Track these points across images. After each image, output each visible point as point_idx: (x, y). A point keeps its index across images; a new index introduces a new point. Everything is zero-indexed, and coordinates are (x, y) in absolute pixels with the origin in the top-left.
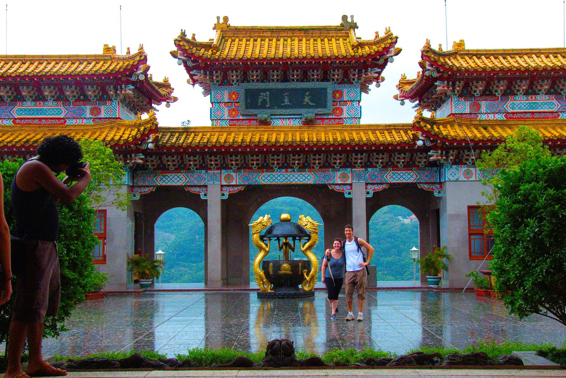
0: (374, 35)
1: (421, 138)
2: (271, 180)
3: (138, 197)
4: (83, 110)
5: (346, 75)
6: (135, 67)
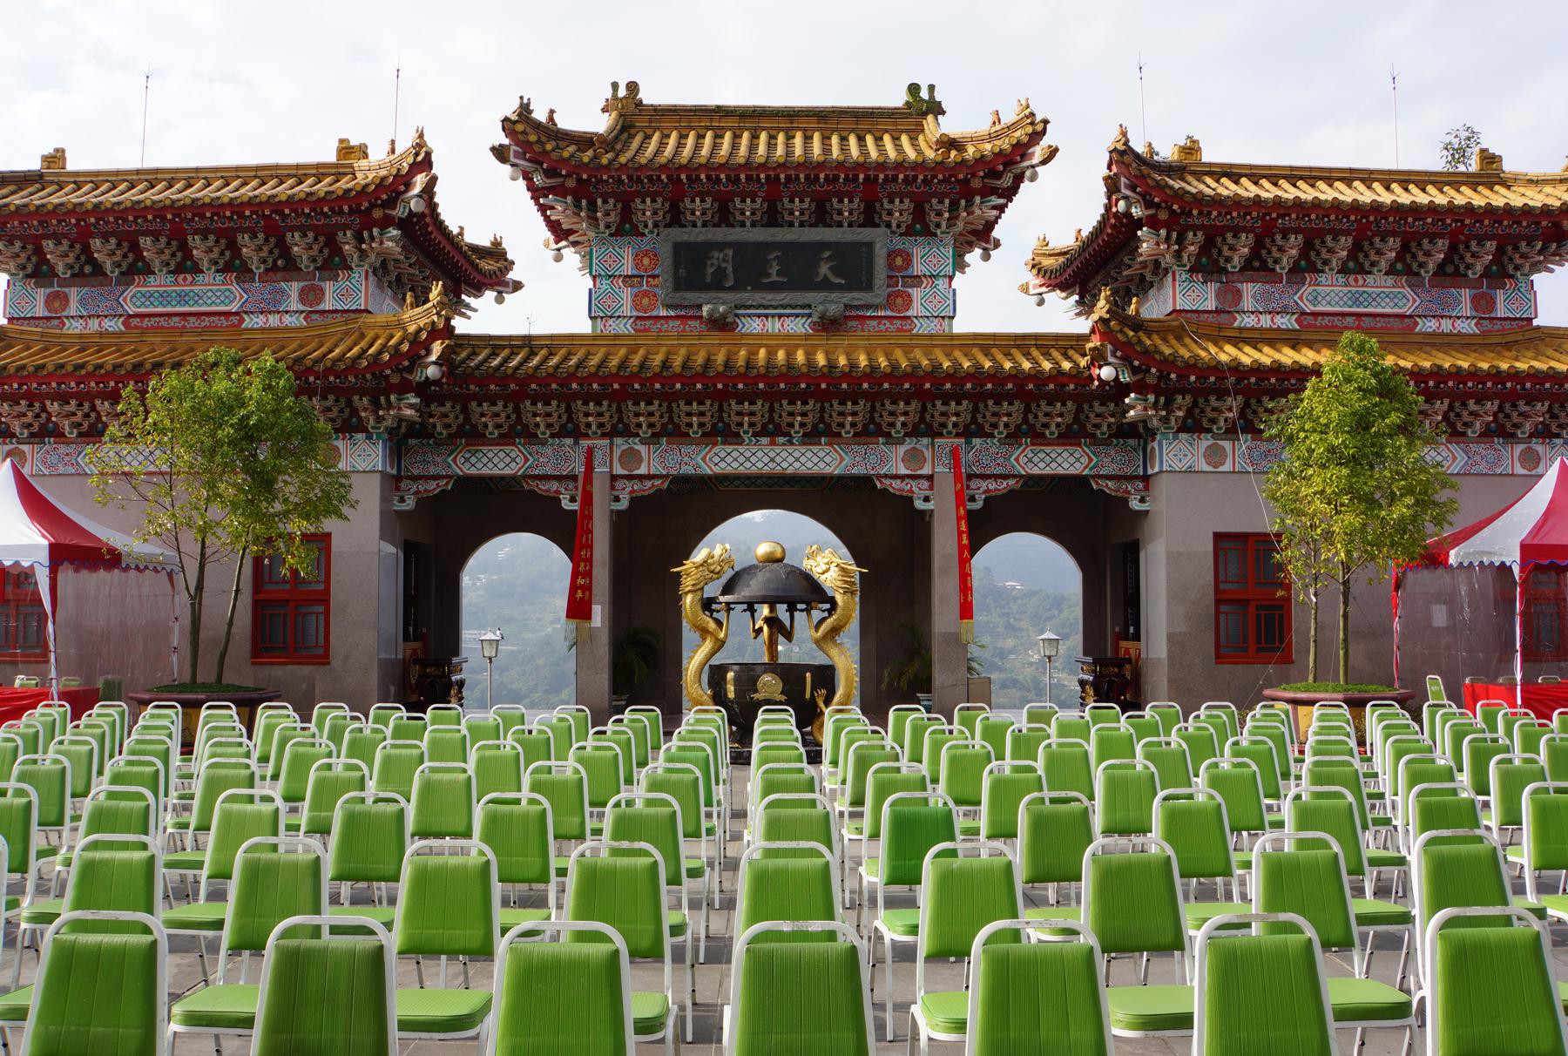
0: (991, 119)
1: (1111, 359)
2: (735, 465)
3: (410, 504)
4: (283, 292)
5: (919, 214)
6: (404, 180)
